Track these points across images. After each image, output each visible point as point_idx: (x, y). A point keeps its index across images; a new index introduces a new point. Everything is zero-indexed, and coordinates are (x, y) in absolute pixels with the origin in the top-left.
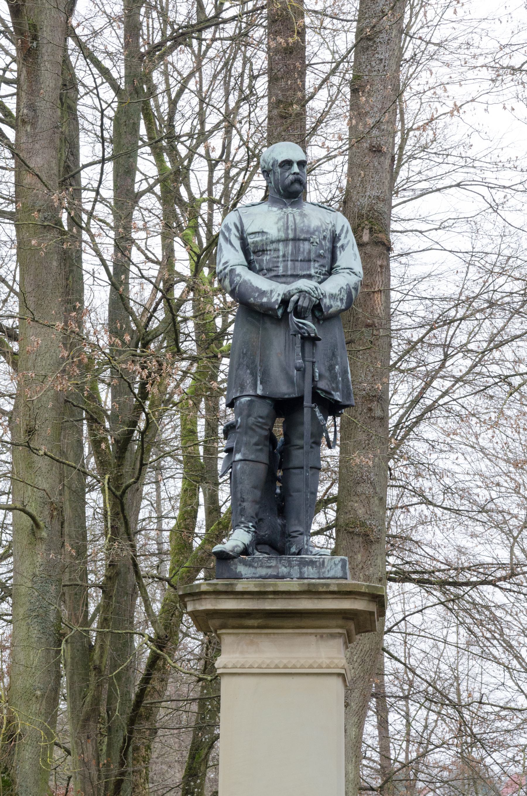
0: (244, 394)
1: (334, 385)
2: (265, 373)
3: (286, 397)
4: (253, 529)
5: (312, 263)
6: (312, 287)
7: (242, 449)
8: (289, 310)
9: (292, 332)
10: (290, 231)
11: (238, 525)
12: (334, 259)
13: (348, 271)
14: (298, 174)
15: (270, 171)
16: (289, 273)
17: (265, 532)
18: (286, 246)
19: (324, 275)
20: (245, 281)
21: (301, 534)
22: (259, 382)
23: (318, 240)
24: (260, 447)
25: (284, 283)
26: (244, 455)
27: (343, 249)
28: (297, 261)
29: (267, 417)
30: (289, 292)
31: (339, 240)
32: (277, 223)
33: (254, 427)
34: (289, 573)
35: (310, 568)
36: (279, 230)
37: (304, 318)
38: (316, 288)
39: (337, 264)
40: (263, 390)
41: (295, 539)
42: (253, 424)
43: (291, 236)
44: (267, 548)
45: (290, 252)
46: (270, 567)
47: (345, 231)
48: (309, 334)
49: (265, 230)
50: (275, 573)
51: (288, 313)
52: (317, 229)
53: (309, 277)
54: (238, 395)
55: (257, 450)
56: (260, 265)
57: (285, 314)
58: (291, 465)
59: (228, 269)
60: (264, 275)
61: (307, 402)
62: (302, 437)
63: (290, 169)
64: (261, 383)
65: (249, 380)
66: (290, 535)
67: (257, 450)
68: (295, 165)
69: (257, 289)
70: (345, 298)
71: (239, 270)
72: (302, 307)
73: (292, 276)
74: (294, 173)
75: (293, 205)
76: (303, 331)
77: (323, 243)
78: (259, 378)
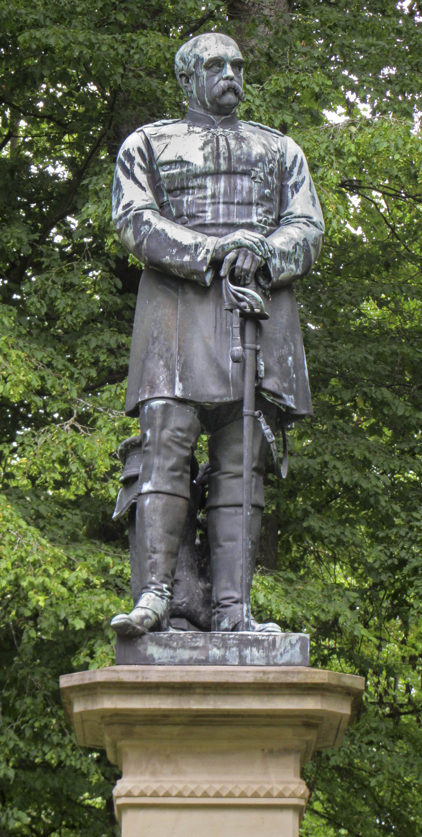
0: (157, 395)
1: (286, 385)
2: (186, 367)
3: (217, 400)
4: (168, 593)
5: (254, 208)
6: (256, 240)
7: (153, 476)
8: (222, 273)
9: (227, 305)
10: (222, 161)
11: (146, 588)
12: (283, 203)
13: (304, 220)
14: (232, 79)
15: (192, 74)
16: (221, 221)
17: (181, 599)
18: (217, 182)
19: (270, 225)
20: (156, 231)
21: (236, 602)
22: (177, 379)
23: (262, 175)
24: (177, 474)
25: (214, 235)
26: (155, 484)
27: (297, 191)
28: (233, 203)
29: (189, 429)
30: (223, 247)
31: (291, 176)
32: (202, 149)
33: (170, 444)
34: (224, 656)
35: (254, 650)
36: (206, 159)
37: (244, 286)
38: (262, 242)
39: (289, 210)
40: (184, 390)
41: (228, 609)
42: (170, 439)
43: (223, 167)
44: (184, 623)
45: (222, 190)
46: (195, 648)
47: (298, 164)
48: (252, 308)
49: (185, 159)
50: (203, 657)
51: (221, 279)
52: (261, 159)
53: (251, 227)
54: (147, 397)
55: (174, 478)
56: (177, 210)
57: (217, 279)
58: (221, 501)
59: (132, 213)
60: (184, 224)
61: (247, 409)
62: (239, 460)
63: (220, 71)
64: (181, 380)
65: (162, 377)
66: (218, 604)
67: (174, 478)
68: (228, 66)
69: (175, 244)
70: (301, 259)
71: (148, 215)
72: (242, 270)
73: (225, 225)
74: (227, 78)
75: (224, 124)
76: (243, 304)
77: (270, 178)
78: (177, 373)
